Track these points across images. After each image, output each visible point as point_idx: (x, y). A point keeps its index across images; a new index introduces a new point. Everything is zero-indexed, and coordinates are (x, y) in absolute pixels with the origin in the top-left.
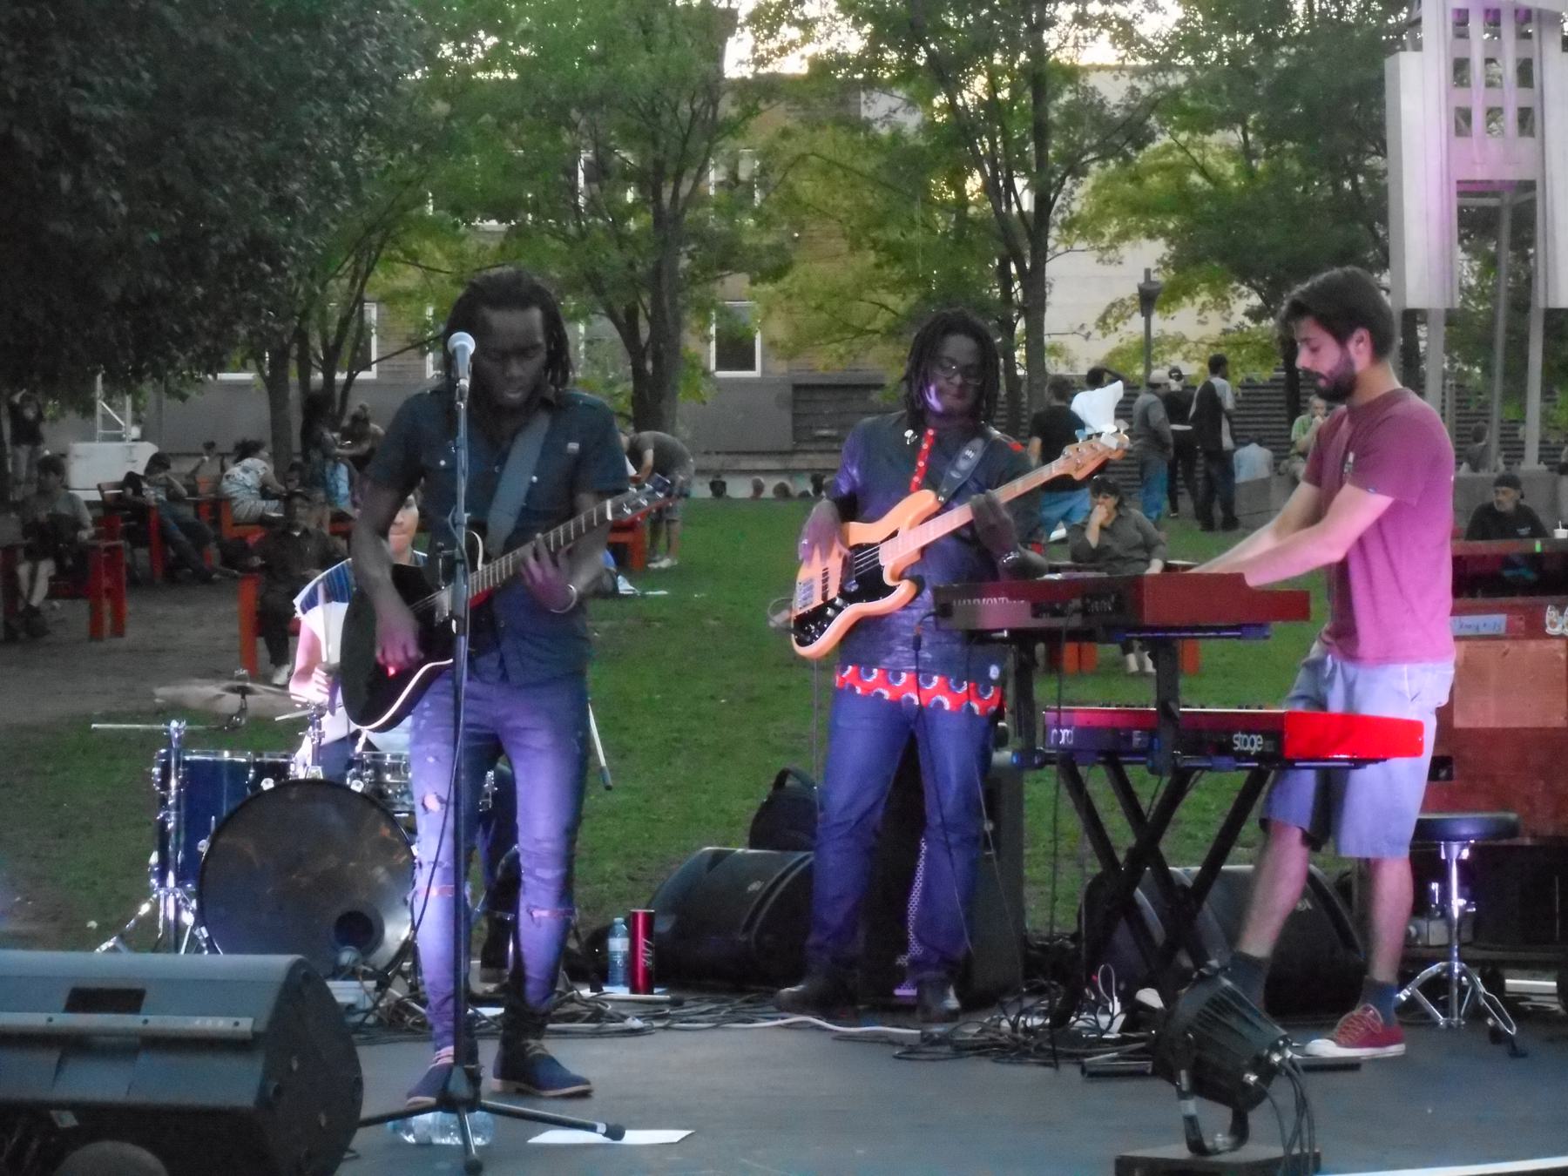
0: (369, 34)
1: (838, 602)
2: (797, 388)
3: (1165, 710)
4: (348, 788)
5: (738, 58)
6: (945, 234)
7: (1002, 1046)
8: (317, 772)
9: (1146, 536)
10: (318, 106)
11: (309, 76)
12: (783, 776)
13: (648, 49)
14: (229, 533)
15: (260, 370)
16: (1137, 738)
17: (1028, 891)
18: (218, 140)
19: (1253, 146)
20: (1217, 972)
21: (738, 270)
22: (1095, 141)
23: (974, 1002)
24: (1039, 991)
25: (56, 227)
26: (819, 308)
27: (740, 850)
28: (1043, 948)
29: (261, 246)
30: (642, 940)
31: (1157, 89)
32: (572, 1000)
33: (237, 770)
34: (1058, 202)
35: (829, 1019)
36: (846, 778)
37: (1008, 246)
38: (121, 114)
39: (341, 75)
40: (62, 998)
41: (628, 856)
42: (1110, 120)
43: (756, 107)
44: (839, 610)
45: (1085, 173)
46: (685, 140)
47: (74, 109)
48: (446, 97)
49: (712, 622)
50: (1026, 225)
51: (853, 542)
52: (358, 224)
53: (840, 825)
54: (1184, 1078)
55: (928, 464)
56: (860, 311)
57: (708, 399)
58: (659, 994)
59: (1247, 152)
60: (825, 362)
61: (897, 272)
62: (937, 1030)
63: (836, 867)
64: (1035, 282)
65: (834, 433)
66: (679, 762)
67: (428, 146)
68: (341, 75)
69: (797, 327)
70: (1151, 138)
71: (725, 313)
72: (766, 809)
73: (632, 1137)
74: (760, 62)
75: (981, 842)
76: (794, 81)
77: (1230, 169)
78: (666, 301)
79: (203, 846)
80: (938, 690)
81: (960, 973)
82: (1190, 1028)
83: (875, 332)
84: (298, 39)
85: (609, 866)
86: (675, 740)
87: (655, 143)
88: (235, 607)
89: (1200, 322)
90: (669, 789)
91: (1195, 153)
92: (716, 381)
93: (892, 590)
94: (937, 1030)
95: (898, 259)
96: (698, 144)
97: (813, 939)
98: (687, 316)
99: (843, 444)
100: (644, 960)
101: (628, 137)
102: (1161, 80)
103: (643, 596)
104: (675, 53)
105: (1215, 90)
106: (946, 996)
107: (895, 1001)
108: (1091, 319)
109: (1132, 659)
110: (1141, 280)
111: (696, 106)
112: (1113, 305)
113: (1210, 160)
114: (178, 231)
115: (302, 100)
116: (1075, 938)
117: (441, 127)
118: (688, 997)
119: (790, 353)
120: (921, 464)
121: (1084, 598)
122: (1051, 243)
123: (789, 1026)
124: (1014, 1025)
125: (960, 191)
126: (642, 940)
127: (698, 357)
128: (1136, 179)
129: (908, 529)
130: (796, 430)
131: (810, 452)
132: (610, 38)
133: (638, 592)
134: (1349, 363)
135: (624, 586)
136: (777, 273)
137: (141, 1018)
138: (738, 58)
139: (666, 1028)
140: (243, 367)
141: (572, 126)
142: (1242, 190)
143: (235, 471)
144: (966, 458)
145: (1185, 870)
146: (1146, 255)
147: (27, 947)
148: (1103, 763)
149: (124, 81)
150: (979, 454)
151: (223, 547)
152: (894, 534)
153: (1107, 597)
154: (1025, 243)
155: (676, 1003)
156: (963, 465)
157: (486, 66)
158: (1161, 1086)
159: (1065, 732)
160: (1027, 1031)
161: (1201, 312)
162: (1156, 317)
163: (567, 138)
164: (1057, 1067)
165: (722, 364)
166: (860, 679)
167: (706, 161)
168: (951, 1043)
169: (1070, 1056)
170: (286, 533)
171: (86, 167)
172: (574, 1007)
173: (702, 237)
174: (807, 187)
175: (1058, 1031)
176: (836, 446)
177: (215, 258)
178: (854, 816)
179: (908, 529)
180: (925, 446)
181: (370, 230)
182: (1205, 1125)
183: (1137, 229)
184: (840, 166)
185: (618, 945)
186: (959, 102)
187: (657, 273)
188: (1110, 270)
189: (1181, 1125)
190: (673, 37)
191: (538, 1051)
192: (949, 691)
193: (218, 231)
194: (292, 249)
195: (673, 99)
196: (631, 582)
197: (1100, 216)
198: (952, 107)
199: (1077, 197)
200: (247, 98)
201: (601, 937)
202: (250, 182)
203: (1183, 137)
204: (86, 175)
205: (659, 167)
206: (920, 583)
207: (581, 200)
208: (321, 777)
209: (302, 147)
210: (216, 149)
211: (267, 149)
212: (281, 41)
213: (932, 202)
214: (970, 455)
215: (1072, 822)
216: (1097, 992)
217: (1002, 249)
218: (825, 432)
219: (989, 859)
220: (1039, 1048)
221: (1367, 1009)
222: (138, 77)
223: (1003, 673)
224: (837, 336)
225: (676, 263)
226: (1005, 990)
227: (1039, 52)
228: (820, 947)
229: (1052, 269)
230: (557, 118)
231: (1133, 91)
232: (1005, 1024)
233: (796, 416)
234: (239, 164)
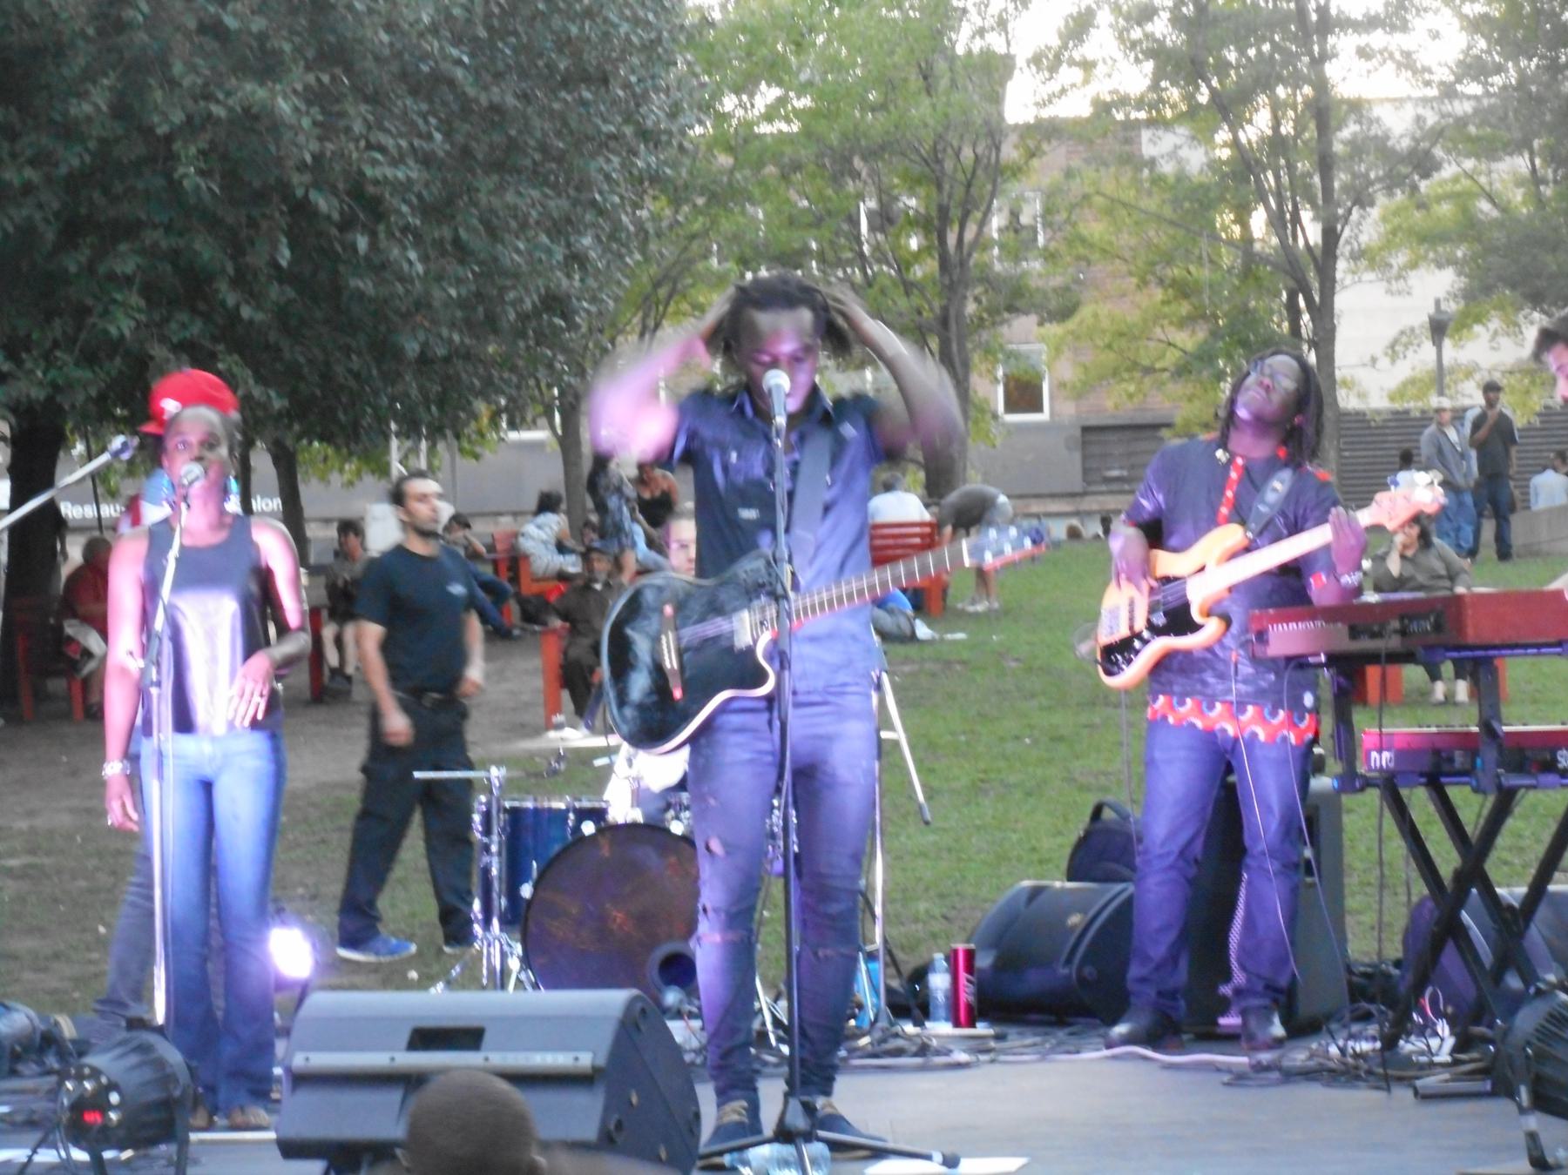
0: (657, 90)
1: (1146, 634)
2: (1086, 430)
3: (1488, 729)
4: (668, 831)
5: (1020, 103)
6: (1230, 270)
7: (1331, 1071)
8: (637, 816)
9: (1448, 566)
10: (608, 161)
11: (599, 132)
12: (1097, 813)
13: (929, 93)
14: (528, 588)
15: (552, 427)
16: (1459, 758)
17: (1349, 920)
18: (510, 197)
19: (1541, 172)
20: (1553, 987)
21: (1026, 313)
22: (1381, 173)
23: (1300, 1029)
24: (1366, 1017)
25: (356, 283)
26: (1109, 346)
27: (1058, 884)
28: (1365, 975)
29: (555, 303)
30: (963, 975)
31: (1443, 116)
32: (896, 1035)
33: (561, 815)
34: (1347, 233)
35: (1155, 1048)
36: (1164, 812)
37: (1297, 281)
38: (414, 175)
39: (628, 130)
40: (405, 1037)
41: (942, 896)
42: (1393, 151)
43: (1038, 148)
44: (1145, 642)
45: (1372, 204)
46: (969, 185)
47: (369, 171)
48: (730, 149)
49: (1013, 664)
50: (1315, 259)
52: (645, 279)
53: (1161, 856)
54: (1524, 1095)
55: (1236, 496)
56: (1146, 353)
57: (998, 442)
58: (982, 1029)
59: (1536, 179)
60: (1114, 403)
61: (1185, 308)
62: (1265, 1057)
63: (1157, 895)
64: (1324, 313)
65: (1125, 473)
66: (987, 802)
67: (713, 198)
68: (628, 130)
69: (1085, 368)
70: (1437, 166)
71: (1010, 355)
72: (1083, 844)
74: (1042, 104)
75: (1302, 870)
76: (1077, 122)
77: (1518, 196)
78: (954, 347)
79: (526, 891)
80: (1252, 721)
81: (1285, 1000)
82: (1529, 1043)
83: (1165, 370)
84: (587, 95)
85: (922, 906)
86: (982, 781)
87: (939, 187)
88: (536, 662)
89: (1493, 348)
90: (978, 828)
91: (1483, 180)
92: (1004, 424)
93: (1194, 628)
94: (1265, 1057)
95: (1186, 296)
96: (983, 186)
97: (1135, 971)
98: (976, 358)
99: (1144, 481)
100: (967, 994)
101: (912, 184)
102: (1447, 107)
103: (942, 640)
104: (956, 97)
105: (1504, 119)
106: (1271, 1023)
107: (1219, 1031)
108: (1378, 349)
109: (1440, 689)
110: (1432, 310)
111: (979, 150)
112: (1403, 333)
113: (1498, 186)
114: (473, 288)
115: (593, 156)
116: (1398, 964)
117: (725, 179)
118: (1012, 1031)
119: (1079, 393)
120: (1229, 494)
121: (1402, 618)
122: (1339, 275)
123: (1115, 1057)
124: (1343, 1051)
125: (1245, 226)
126: (963, 975)
127: (986, 400)
128: (1422, 206)
129: (1214, 565)
130: (1086, 471)
131: (1101, 493)
132: (890, 85)
133: (937, 636)
135: (923, 631)
136: (1064, 314)
138: (1020, 103)
139: (993, 1061)
140: (533, 425)
141: (856, 175)
142: (1530, 217)
143: (530, 528)
144: (1275, 490)
145: (1512, 892)
146: (1436, 285)
148: (1426, 785)
149: (416, 142)
150: (1288, 484)
151: (522, 602)
152: (1202, 569)
153: (1426, 617)
154: (1310, 279)
155: (999, 1037)
156: (1271, 497)
157: (769, 117)
158: (1504, 1106)
159: (1386, 755)
160: (1356, 1056)
161: (1493, 338)
162: (1447, 343)
163: (851, 186)
164: (1388, 1090)
165: (1011, 407)
166: (1172, 708)
167: (991, 202)
168: (1280, 1069)
169: (1400, 1079)
170: (587, 587)
171: (381, 228)
172: (900, 1043)
173: (987, 279)
174: (1095, 228)
175: (1387, 1054)
176: (1126, 487)
177: (512, 316)
178: (1175, 847)
179: (1214, 565)
181: (657, 285)
182: (1545, 1139)
183: (1425, 258)
184: (1125, 205)
185: (939, 982)
186: (1243, 139)
187: (944, 321)
188: (1398, 301)
189: (1521, 1140)
190: (953, 83)
191: (829, 1110)
192: (1263, 721)
193: (514, 287)
194: (585, 304)
195: (955, 143)
196: (929, 626)
197: (1389, 243)
198: (1235, 144)
199: (1365, 228)
200: (538, 157)
201: (920, 975)
202: (544, 239)
203: (1469, 164)
204: (382, 236)
205: (943, 212)
206: (1227, 620)
207: (866, 248)
208: (640, 819)
209: (594, 203)
210: (508, 207)
211: (558, 205)
212: (569, 98)
213: (1219, 239)
214: (1279, 486)
215: (1397, 847)
216: (1423, 1015)
217: (1292, 284)
218: (1115, 473)
219: (1313, 885)
220: (1370, 1072)
222: (430, 137)
223: (1317, 699)
224: (1126, 376)
225: (962, 305)
226: (1329, 1017)
227: (1322, 85)
228: (1143, 980)
229: (1341, 301)
230: (839, 166)
231: (1419, 119)
232: (1334, 1050)
233: (1085, 458)
234: (531, 221)
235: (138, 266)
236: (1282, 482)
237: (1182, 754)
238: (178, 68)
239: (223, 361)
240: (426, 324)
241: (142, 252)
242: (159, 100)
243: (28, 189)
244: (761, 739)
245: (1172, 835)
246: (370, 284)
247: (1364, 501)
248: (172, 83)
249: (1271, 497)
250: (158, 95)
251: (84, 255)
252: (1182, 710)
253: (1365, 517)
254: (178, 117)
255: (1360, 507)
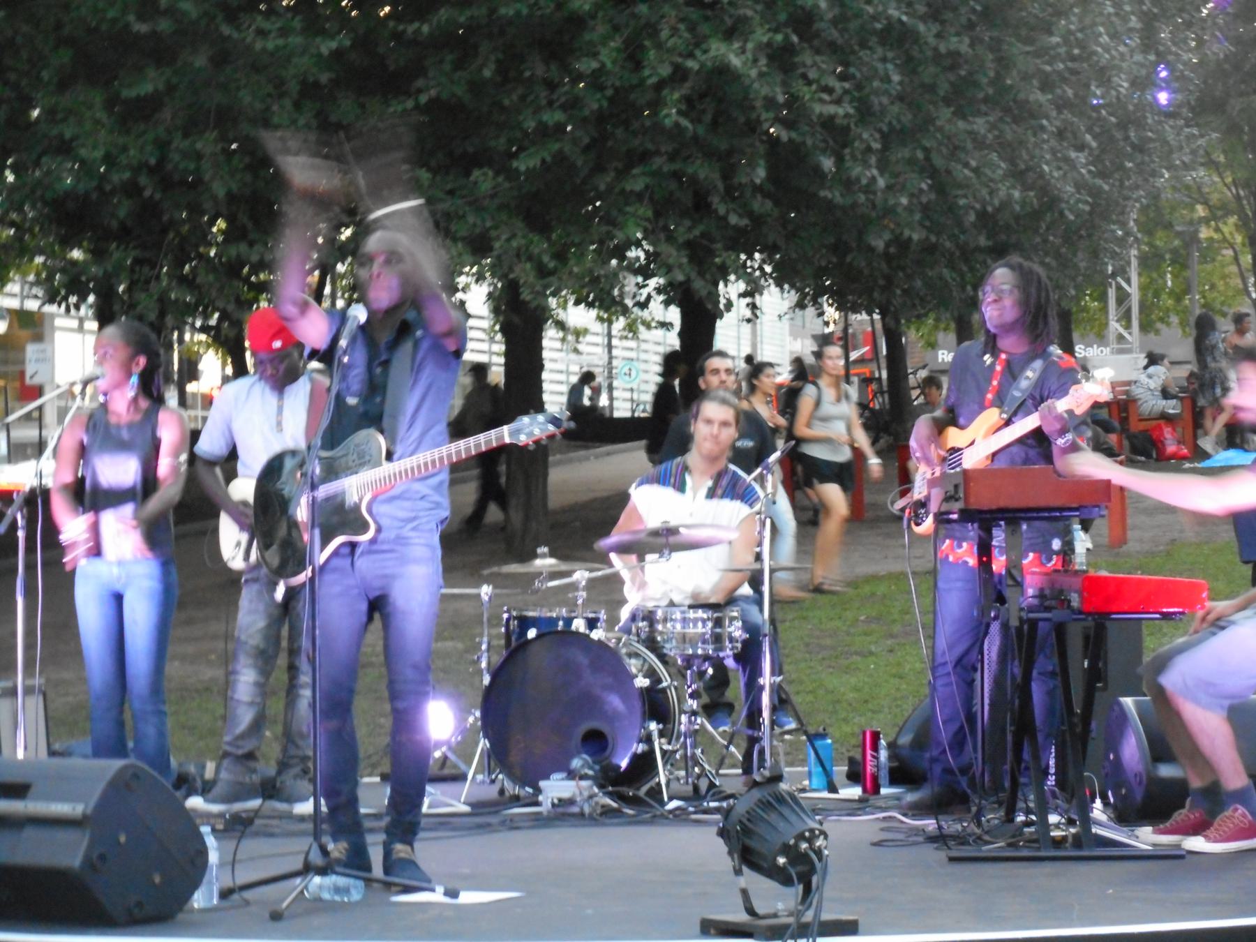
14: (1135, 426)
51: (949, 446)
55: (1000, 384)
120: (995, 383)
144: (1027, 378)
152: (972, 443)
156: (1024, 384)
180: (998, 368)
221: (1236, 810)
237: (959, 584)
239: (720, 256)
240: (892, 226)
242: (652, 57)
245: (951, 647)
246: (837, 194)
248: (659, 46)
250: (652, 54)
251: (609, 177)
252: (959, 551)
254: (665, 71)
255: (1059, 398)
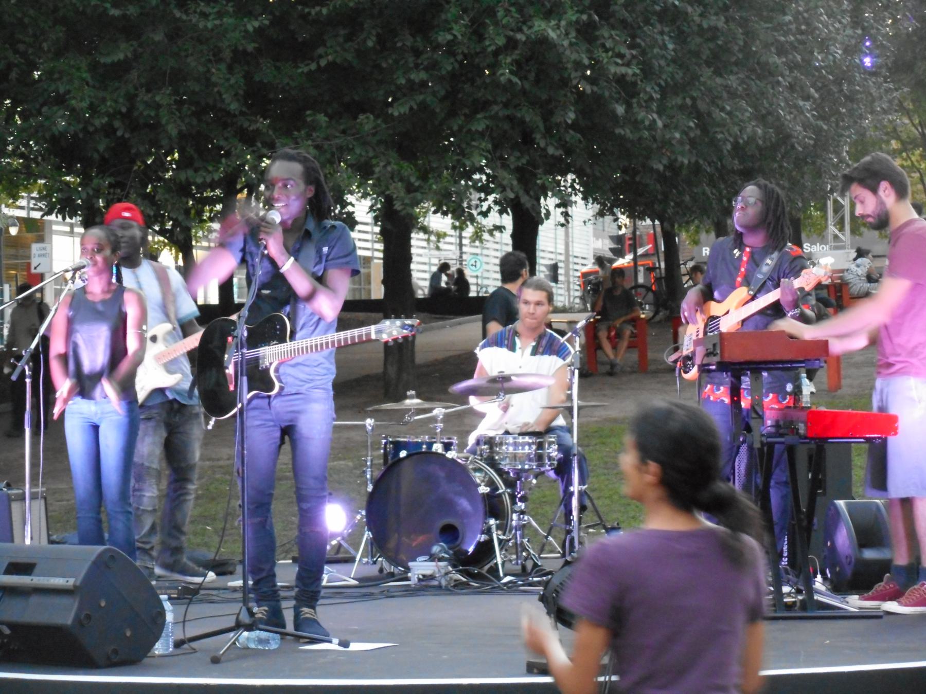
73: (354, 647)
120: (743, 270)
134: (881, 203)
137: (31, 577)
144: (767, 264)
147: (769, 500)
152: (727, 313)
156: (765, 269)
180: (745, 259)
214: (769, 262)
235: (487, 127)
236: (772, 259)
238: (500, 14)
239: (541, 179)
241: (491, 118)
243: (423, 84)
244: (266, 413)
246: (628, 131)
247: (797, 274)
248: (497, 24)
249: (765, 269)
251: (460, 120)
253: (797, 283)
254: (501, 41)
